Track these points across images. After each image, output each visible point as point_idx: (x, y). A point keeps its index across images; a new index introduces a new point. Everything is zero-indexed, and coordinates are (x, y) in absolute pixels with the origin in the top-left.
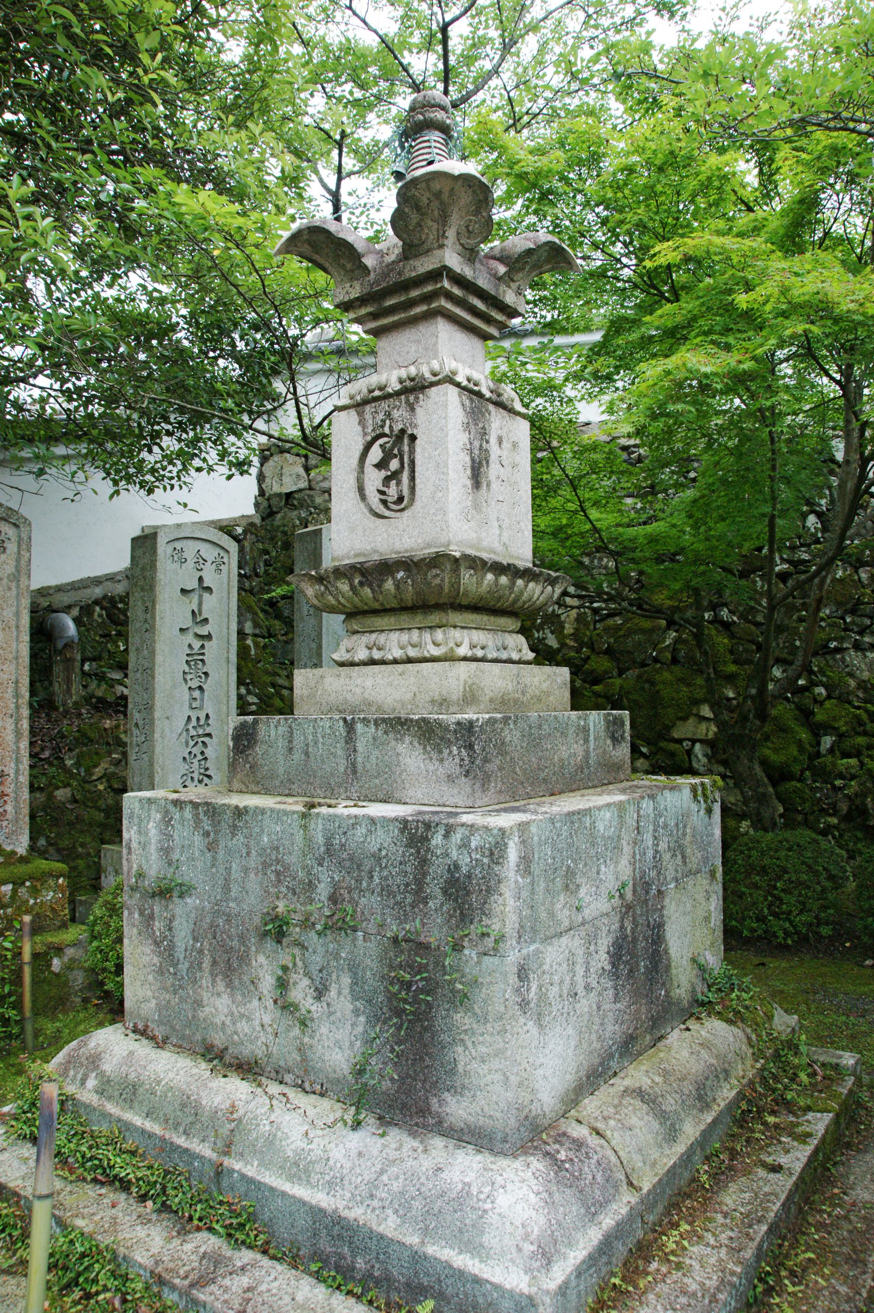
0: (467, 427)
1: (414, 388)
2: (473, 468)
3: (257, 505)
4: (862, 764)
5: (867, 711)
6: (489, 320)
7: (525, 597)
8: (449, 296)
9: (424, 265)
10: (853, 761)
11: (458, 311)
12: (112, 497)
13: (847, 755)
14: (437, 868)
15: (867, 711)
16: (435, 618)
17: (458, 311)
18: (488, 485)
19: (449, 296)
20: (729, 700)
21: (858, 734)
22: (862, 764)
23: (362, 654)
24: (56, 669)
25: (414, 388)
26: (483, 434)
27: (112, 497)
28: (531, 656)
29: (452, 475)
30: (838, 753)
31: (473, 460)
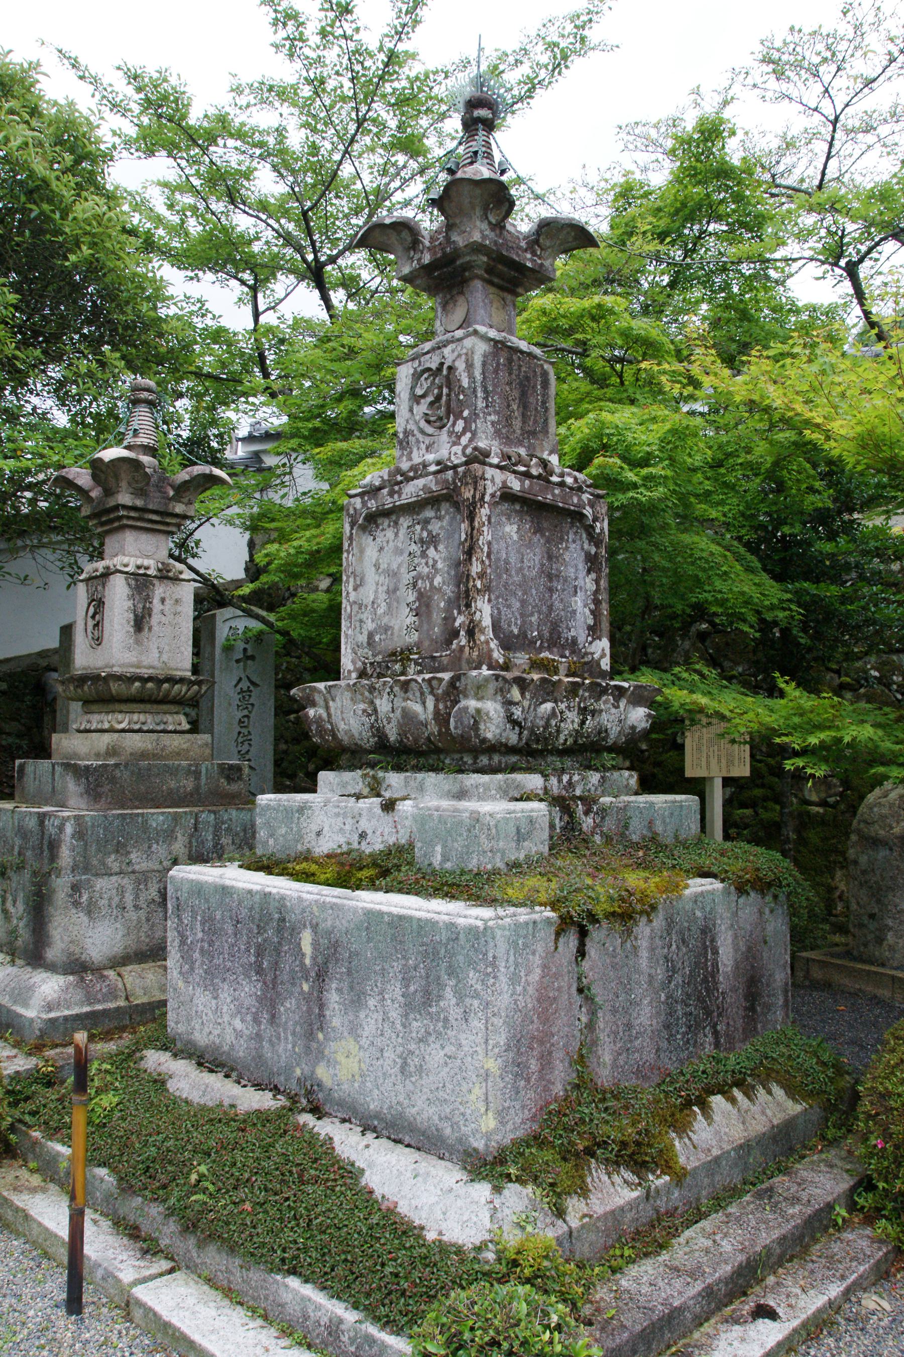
0: (131, 597)
1: (107, 574)
2: (136, 621)
3: (247, 570)
4: (757, 813)
5: (767, 765)
6: (168, 524)
7: (173, 693)
8: (129, 518)
9: (111, 503)
10: (748, 812)
11: (139, 524)
12: (69, 587)
13: (743, 806)
14: (46, 837)
15: (767, 765)
16: (111, 707)
17: (139, 524)
18: (150, 629)
19: (129, 518)
20: (643, 751)
21: (757, 786)
22: (757, 813)
23: (106, 726)
24: (46, 719)
25: (107, 574)
26: (148, 599)
27: (69, 587)
28: (188, 727)
29: (116, 627)
30: (735, 803)
31: (136, 616)
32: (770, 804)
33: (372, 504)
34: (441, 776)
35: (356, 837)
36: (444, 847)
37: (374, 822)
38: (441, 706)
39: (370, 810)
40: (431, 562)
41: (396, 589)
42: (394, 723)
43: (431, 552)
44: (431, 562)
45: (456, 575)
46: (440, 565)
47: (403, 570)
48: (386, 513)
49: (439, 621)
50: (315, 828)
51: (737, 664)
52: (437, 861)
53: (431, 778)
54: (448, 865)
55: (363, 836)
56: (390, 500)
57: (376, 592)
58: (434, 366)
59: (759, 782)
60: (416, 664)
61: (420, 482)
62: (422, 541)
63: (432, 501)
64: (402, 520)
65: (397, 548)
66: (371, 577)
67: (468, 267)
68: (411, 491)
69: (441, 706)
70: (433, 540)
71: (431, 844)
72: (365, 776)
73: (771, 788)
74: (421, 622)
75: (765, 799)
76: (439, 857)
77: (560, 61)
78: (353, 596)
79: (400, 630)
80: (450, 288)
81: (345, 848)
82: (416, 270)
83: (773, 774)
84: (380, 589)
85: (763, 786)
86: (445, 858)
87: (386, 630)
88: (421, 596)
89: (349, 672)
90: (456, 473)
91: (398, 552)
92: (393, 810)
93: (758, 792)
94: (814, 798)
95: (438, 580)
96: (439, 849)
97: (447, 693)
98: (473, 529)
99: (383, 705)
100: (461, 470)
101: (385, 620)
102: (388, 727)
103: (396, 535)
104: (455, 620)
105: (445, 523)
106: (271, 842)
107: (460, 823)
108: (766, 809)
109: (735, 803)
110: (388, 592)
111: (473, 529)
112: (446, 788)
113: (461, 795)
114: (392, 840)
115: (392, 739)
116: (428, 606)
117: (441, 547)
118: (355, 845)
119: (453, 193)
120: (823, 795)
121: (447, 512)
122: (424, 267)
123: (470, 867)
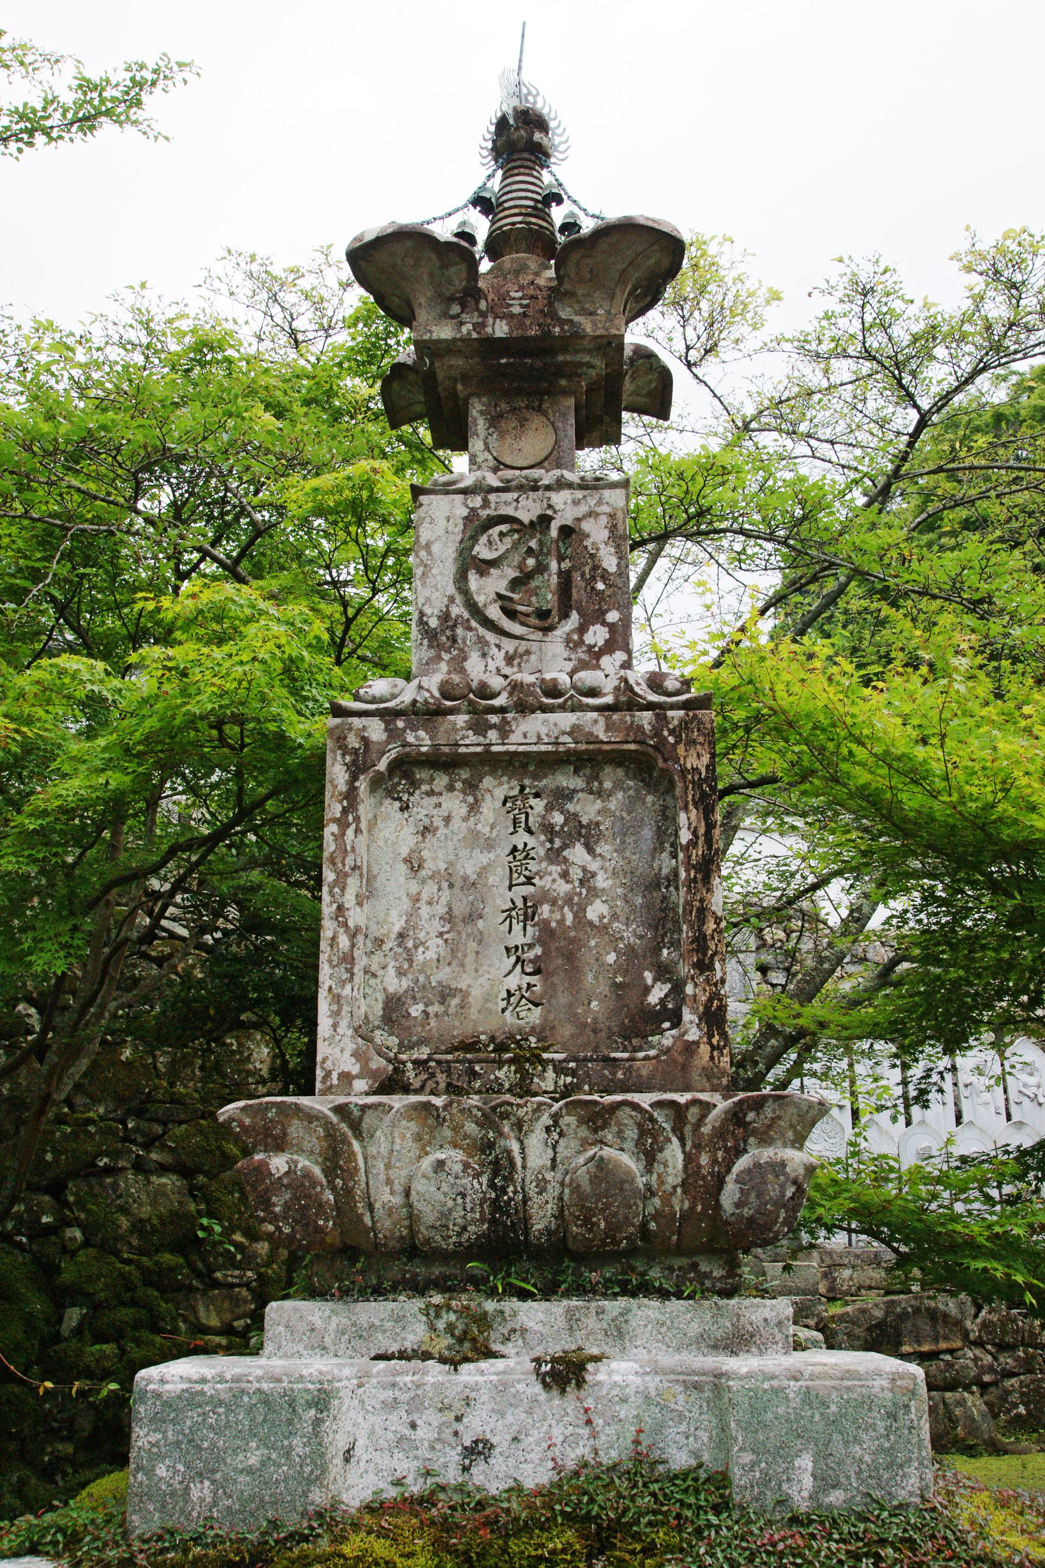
4: (123, 1351)
5: (139, 1266)
10: (109, 1348)
13: (101, 1338)
15: (139, 1266)
21: (123, 1303)
22: (123, 1351)
30: (87, 1335)
32: (145, 1335)
33: (421, 740)
34: (675, 1305)
35: (454, 1456)
36: (822, 1456)
37: (515, 1417)
38: (704, 1159)
39: (501, 1388)
40: (576, 874)
41: (472, 917)
42: (553, 1190)
43: (578, 854)
44: (576, 874)
45: (648, 906)
46: (602, 881)
47: (498, 878)
48: (445, 762)
49: (604, 988)
50: (342, 1443)
51: (96, 1100)
52: (801, 1489)
53: (646, 1311)
54: (835, 1497)
55: (478, 1450)
56: (472, 738)
57: (412, 915)
58: (525, 517)
59: (127, 1296)
60: (560, 1069)
61: (566, 720)
62: (549, 830)
63: (587, 759)
64: (487, 782)
65: (474, 834)
66: (395, 882)
67: (573, 371)
68: (533, 732)
69: (704, 1159)
70: (585, 834)
71: (784, 1453)
72: (433, 1312)
73: (148, 1307)
74: (550, 990)
75: (137, 1325)
76: (808, 1482)
77: (86, 122)
78: (356, 917)
79: (488, 998)
80: (508, 394)
81: (416, 1487)
82: (466, 340)
83: (148, 1283)
84: (425, 911)
85: (134, 1303)
86: (825, 1481)
87: (443, 999)
88: (547, 934)
89: (346, 1078)
90: (662, 719)
91: (476, 841)
92: (580, 1384)
93: (125, 1314)
94: (214, 1322)
95: (596, 911)
96: (805, 1462)
97: (720, 1133)
98: (710, 826)
99: (534, 1152)
100: (676, 715)
101: (442, 975)
102: (536, 1200)
103: (474, 808)
104: (647, 990)
105: (613, 805)
106: (201, 1491)
107: (867, 1402)
108: (137, 1341)
109: (87, 1335)
110: (449, 917)
111: (710, 826)
112: (694, 1329)
113: (738, 1341)
114: (571, 1458)
115: (538, 1226)
116: (570, 957)
117: (604, 848)
118: (452, 1476)
119: (603, 245)
120: (228, 1316)
121: (618, 785)
122: (490, 346)
123: (902, 1495)
